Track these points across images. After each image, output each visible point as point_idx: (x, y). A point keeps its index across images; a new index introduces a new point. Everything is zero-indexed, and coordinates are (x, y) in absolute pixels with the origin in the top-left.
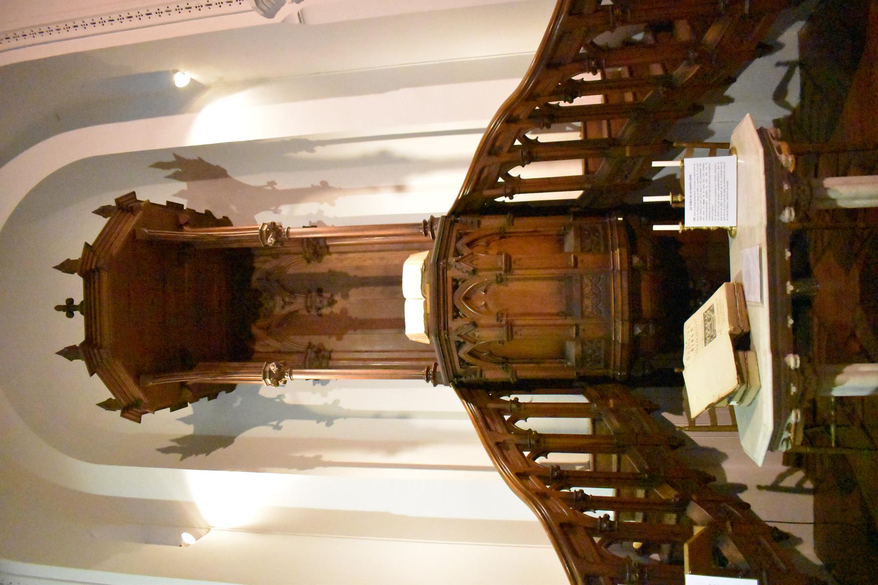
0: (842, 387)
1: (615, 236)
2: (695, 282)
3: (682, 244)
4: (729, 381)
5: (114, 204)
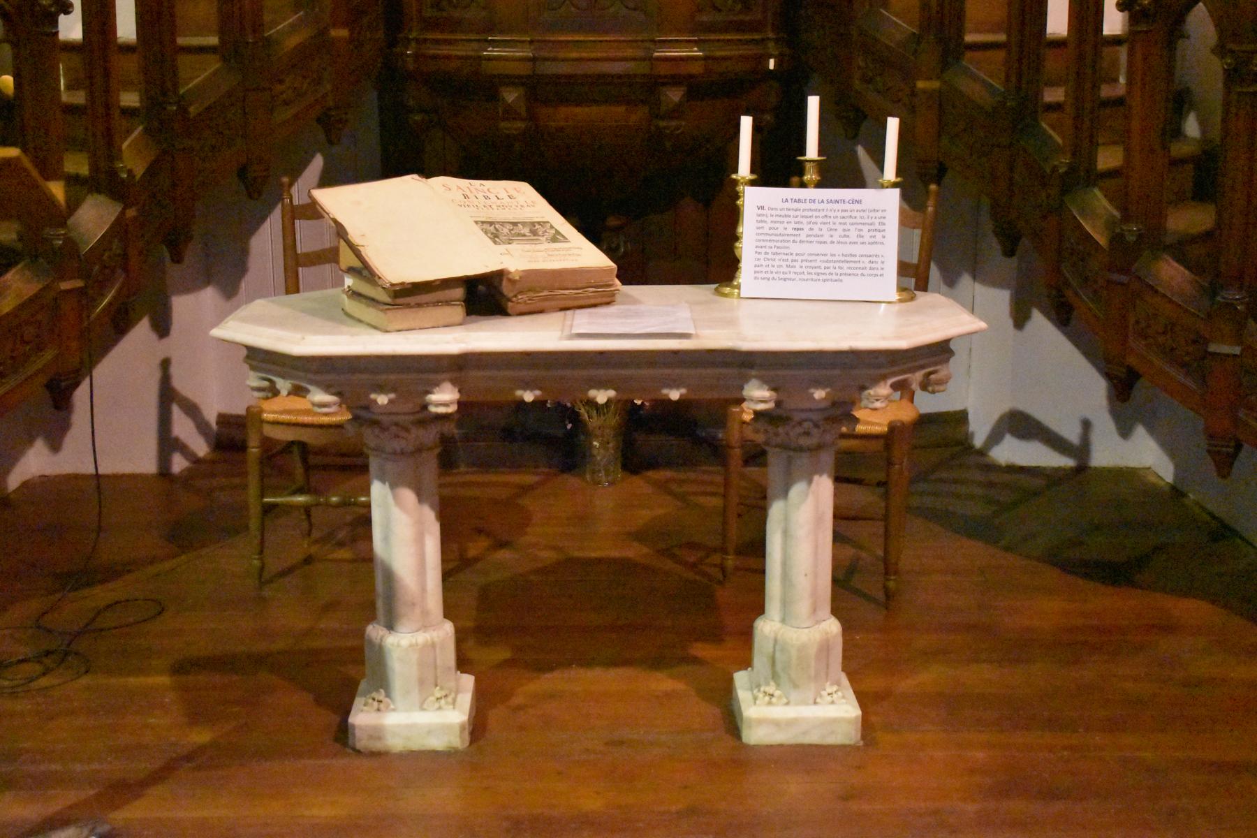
0: (390, 497)
1: (731, 51)
2: (617, 230)
3: (707, 204)
4: (397, 267)
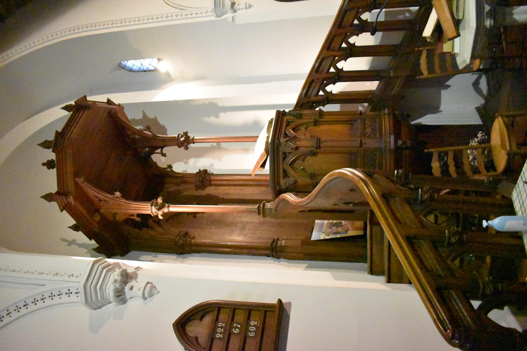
5: (74, 104)
